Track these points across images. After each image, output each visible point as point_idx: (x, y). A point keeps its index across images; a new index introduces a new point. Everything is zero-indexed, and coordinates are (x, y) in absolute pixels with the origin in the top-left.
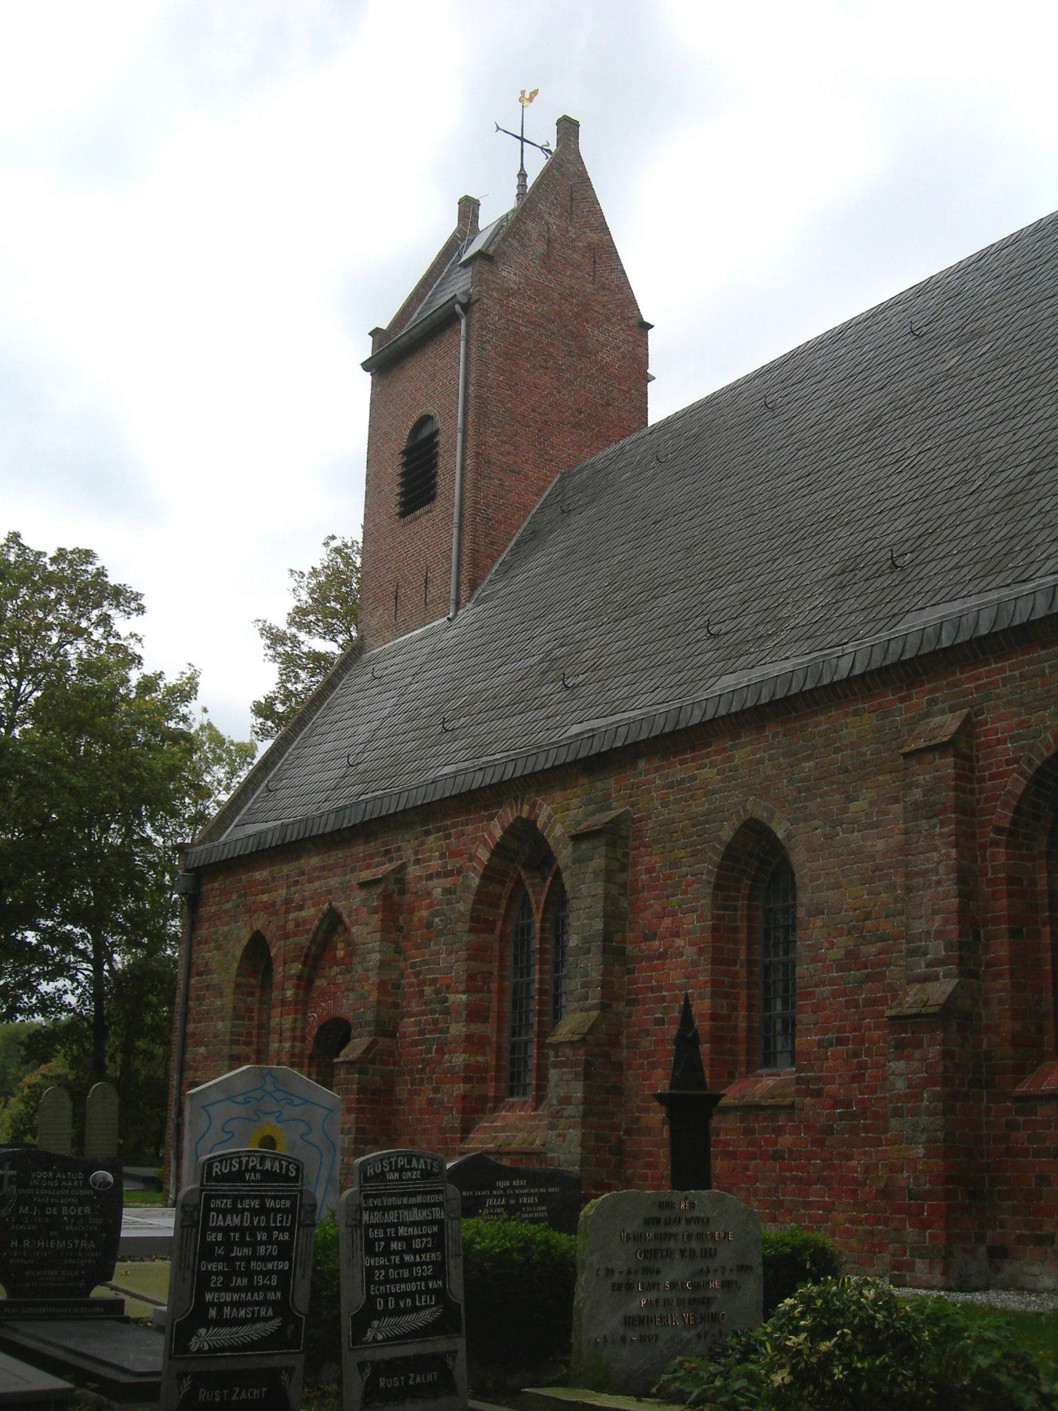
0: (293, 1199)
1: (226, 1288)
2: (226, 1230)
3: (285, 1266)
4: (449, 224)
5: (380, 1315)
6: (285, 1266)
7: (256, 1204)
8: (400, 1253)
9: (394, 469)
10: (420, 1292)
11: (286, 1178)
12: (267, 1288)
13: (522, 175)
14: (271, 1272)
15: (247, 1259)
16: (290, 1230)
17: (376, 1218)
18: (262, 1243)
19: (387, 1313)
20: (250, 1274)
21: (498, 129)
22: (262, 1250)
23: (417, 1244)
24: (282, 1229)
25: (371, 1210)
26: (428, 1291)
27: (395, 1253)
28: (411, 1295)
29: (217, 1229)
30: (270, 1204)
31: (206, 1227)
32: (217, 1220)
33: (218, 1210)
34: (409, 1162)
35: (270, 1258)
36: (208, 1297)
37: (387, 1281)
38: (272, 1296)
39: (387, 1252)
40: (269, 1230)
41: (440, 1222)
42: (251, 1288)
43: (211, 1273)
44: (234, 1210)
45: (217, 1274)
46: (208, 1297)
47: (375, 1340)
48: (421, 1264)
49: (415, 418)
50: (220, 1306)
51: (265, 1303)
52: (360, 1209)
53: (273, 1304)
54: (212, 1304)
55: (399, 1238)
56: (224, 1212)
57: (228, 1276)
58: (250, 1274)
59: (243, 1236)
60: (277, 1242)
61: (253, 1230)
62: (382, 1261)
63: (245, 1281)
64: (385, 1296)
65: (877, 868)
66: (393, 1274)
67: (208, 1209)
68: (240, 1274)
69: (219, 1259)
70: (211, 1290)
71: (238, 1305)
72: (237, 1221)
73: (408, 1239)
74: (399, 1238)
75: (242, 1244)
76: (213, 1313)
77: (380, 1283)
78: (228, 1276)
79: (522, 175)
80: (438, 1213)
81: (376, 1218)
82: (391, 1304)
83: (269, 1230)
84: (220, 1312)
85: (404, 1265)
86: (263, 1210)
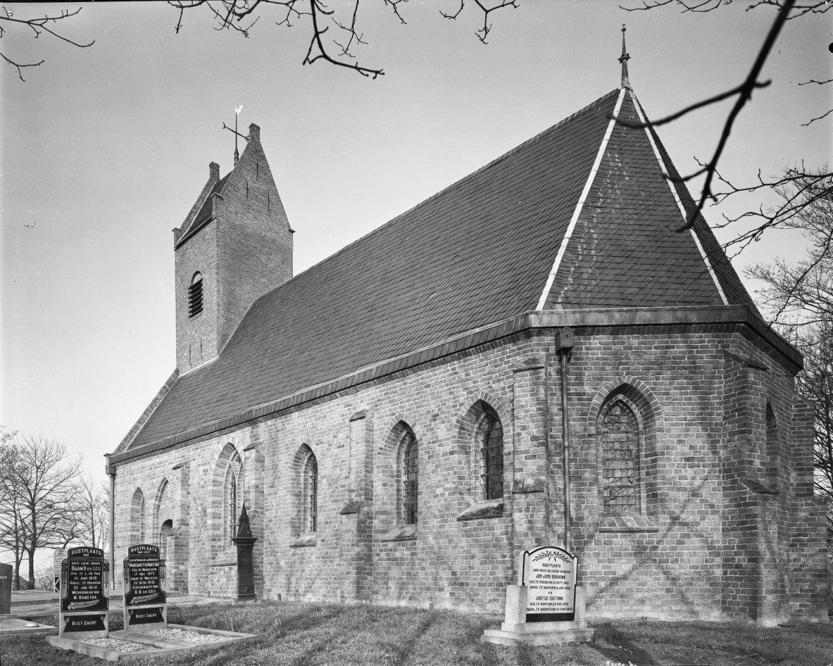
0: (101, 562)
1: (79, 590)
2: (78, 572)
3: (99, 583)
4: (206, 176)
5: (136, 596)
6: (99, 583)
7: (87, 563)
8: (143, 576)
9: (186, 296)
10: (150, 589)
11: (98, 555)
12: (93, 590)
13: (237, 153)
14: (95, 585)
15: (86, 581)
16: (101, 572)
17: (134, 565)
18: (90, 576)
19: (138, 595)
20: (87, 585)
21: (225, 127)
22: (91, 578)
23: (149, 574)
24: (97, 572)
25: (133, 563)
26: (153, 589)
27: (141, 576)
28: (147, 590)
29: (74, 571)
30: (93, 563)
31: (71, 571)
32: (74, 568)
33: (75, 566)
34: (146, 548)
35: (94, 581)
36: (73, 593)
37: (138, 585)
38: (95, 592)
39: (138, 576)
40: (93, 572)
41: (157, 567)
42: (88, 590)
43: (74, 585)
44: (80, 566)
45: (76, 585)
46: (73, 593)
47: (134, 603)
48: (151, 580)
49: (194, 272)
50: (78, 596)
51: (94, 595)
52: (128, 562)
53: (97, 595)
54: (75, 595)
55: (142, 572)
56: (77, 566)
57: (80, 586)
58: (87, 585)
59: (84, 574)
60: (96, 575)
61: (87, 572)
62: (137, 579)
63: (86, 588)
64: (138, 590)
65: (445, 404)
66: (141, 583)
67: (71, 565)
68: (84, 585)
69: (76, 581)
70: (74, 590)
71: (85, 595)
72: (82, 569)
73: (146, 572)
74: (142, 572)
75: (84, 576)
76: (75, 598)
77: (136, 585)
78: (80, 586)
79: (237, 153)
80: (157, 565)
81: (134, 565)
82: (140, 592)
83: (93, 572)
84: (78, 597)
85: (144, 580)
86: (90, 566)
